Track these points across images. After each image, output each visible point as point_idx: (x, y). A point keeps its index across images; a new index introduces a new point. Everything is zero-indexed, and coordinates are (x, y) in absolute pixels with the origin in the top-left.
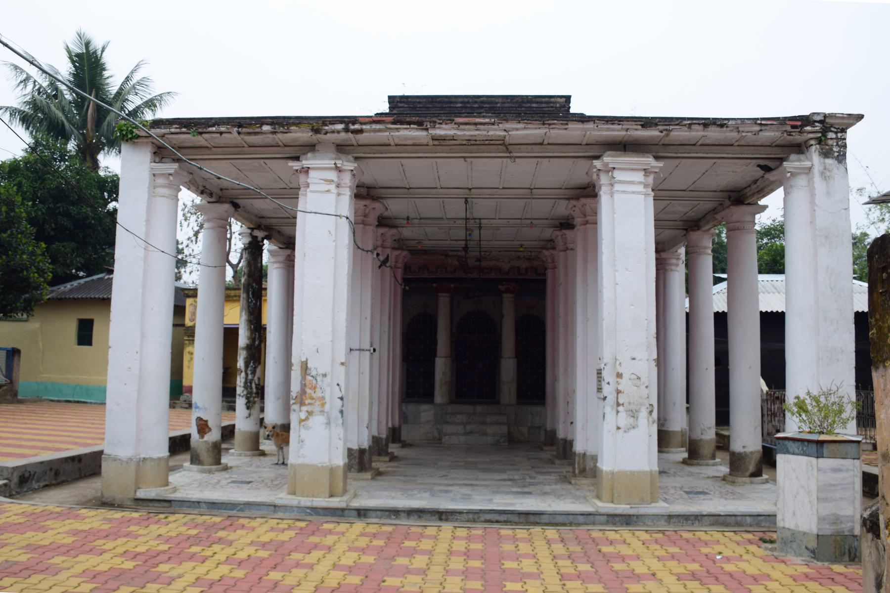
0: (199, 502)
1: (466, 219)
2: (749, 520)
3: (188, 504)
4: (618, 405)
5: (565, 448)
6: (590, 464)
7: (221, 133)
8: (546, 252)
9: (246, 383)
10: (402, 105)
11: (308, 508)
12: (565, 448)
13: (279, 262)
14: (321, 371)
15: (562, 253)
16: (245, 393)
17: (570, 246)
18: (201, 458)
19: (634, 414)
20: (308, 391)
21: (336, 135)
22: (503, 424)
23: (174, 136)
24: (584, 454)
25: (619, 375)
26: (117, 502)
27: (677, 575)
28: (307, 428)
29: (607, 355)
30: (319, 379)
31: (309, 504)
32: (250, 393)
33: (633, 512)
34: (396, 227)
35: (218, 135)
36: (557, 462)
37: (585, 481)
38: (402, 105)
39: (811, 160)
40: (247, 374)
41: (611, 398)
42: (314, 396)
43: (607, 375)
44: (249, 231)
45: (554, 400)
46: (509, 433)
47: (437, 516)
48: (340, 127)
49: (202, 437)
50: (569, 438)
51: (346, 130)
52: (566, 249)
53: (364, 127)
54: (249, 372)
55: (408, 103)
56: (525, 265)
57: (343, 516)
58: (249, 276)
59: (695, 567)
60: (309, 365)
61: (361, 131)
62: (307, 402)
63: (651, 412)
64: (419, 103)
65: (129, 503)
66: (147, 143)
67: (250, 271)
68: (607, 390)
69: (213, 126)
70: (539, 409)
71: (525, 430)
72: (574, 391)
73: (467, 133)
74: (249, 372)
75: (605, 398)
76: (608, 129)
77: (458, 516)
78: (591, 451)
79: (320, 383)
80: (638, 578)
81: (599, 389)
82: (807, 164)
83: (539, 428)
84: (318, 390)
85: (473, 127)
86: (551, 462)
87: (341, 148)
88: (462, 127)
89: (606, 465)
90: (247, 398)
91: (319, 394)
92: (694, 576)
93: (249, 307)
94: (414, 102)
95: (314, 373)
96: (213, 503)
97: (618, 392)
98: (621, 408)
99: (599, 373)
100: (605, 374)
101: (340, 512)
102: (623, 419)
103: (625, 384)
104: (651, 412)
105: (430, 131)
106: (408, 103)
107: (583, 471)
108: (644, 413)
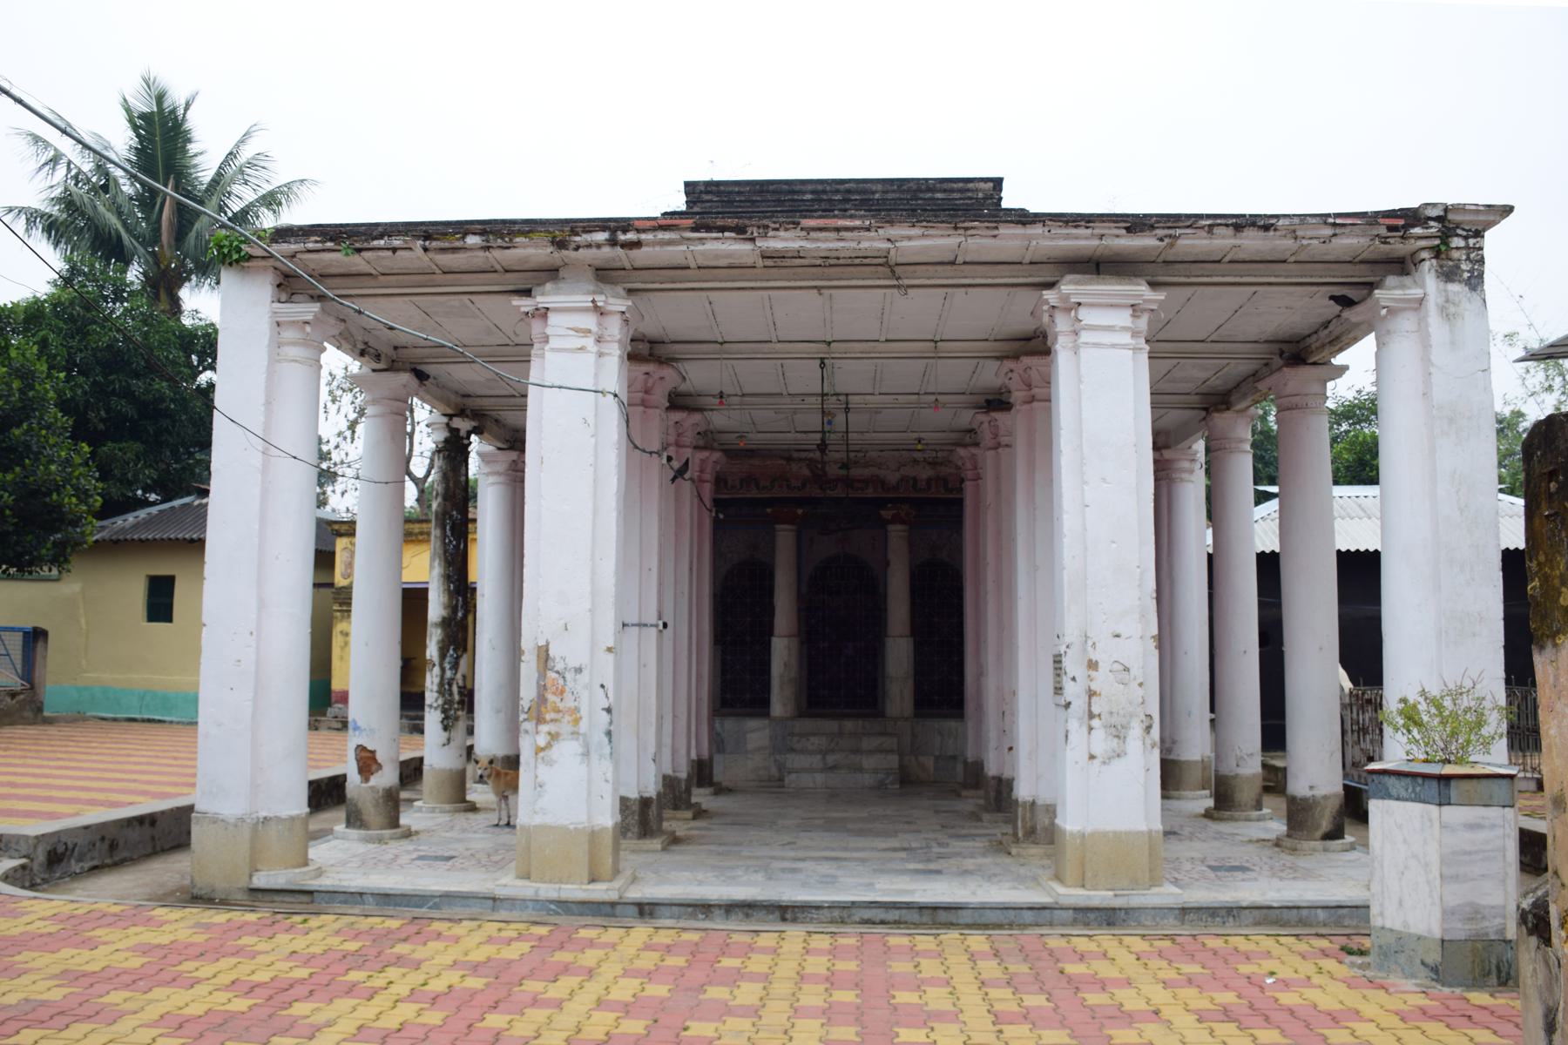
0: (361, 894)
2: (1321, 914)
3: (342, 897)
4: (1091, 716)
5: (999, 792)
6: (1042, 820)
7: (394, 250)
8: (962, 452)
9: (441, 684)
11: (552, 902)
12: (999, 792)
13: (498, 473)
14: (573, 663)
16: (440, 702)
17: (1004, 440)
18: (365, 817)
19: (1118, 733)
20: (551, 697)
21: (594, 250)
25: (1093, 665)
26: (218, 896)
29: (1071, 633)
30: (568, 676)
31: (553, 895)
32: (449, 702)
33: (1118, 903)
34: (701, 410)
35: (390, 253)
37: (1034, 850)
39: (1423, 286)
40: (443, 670)
41: (1079, 704)
42: (561, 706)
43: (1072, 665)
44: (445, 420)
45: (980, 707)
46: (902, 767)
48: (601, 236)
49: (367, 780)
50: (1006, 775)
51: (613, 242)
52: (998, 446)
53: (643, 236)
54: (447, 666)
55: (719, 193)
56: (925, 473)
60: (551, 653)
62: (548, 717)
63: (1148, 728)
64: (739, 193)
65: (239, 896)
66: (265, 268)
67: (447, 489)
68: (1072, 691)
69: (381, 237)
70: (953, 724)
71: (929, 762)
74: (447, 666)
75: (1068, 705)
76: (1067, 237)
78: (1044, 797)
79: (570, 684)
81: (1058, 690)
82: (1416, 292)
83: (954, 758)
84: (567, 695)
85: (833, 235)
86: (975, 817)
87: (604, 274)
88: (813, 235)
89: (1071, 821)
90: (444, 711)
91: (569, 702)
93: (445, 551)
94: (730, 193)
95: (559, 666)
97: (1091, 694)
98: (1095, 723)
99: (1058, 660)
100: (1067, 663)
101: (608, 909)
102: (1101, 741)
103: (1101, 680)
104: (1148, 728)
105: (759, 243)
106: (719, 193)
107: (1031, 832)
108: (1136, 730)
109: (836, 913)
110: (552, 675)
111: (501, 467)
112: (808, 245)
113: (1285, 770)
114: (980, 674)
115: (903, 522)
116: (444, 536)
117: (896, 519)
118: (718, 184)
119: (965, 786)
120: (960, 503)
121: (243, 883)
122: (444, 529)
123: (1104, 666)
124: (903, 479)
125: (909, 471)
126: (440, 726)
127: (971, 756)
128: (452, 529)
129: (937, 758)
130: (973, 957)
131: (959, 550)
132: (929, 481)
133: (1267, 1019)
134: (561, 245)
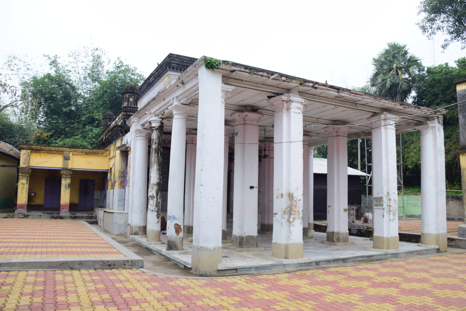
0: (251, 268)
1: (245, 124)
2: (425, 252)
3: (245, 269)
7: (262, 76)
9: (157, 204)
10: (177, 59)
11: (298, 264)
13: (143, 136)
14: (298, 199)
16: (156, 209)
20: (293, 208)
23: (240, 72)
25: (390, 200)
26: (208, 274)
27: (157, 299)
28: (293, 226)
30: (298, 202)
31: (297, 262)
32: (158, 209)
34: (233, 127)
38: (177, 59)
39: (435, 124)
40: (157, 199)
42: (296, 210)
44: (161, 120)
47: (342, 262)
48: (312, 84)
49: (178, 235)
51: (312, 87)
53: (320, 86)
54: (158, 198)
55: (180, 59)
57: (311, 266)
58: (159, 144)
59: (167, 293)
60: (294, 196)
61: (316, 88)
62: (293, 213)
64: (185, 60)
65: (214, 273)
66: (220, 72)
67: (159, 142)
69: (261, 72)
73: (352, 97)
74: (158, 198)
75: (384, 209)
76: (391, 104)
77: (350, 260)
80: (137, 302)
82: (434, 125)
84: (297, 207)
85: (354, 95)
87: (301, 93)
88: (351, 94)
90: (158, 212)
91: (297, 209)
92: (166, 298)
93: (159, 161)
94: (183, 59)
95: (295, 199)
96: (258, 267)
98: (391, 212)
101: (309, 264)
102: (392, 217)
105: (340, 93)
106: (180, 59)
109: (353, 259)
110: (294, 202)
111: (144, 135)
112: (349, 96)
116: (158, 156)
118: (180, 56)
121: (215, 269)
122: (158, 154)
123: (392, 200)
126: (156, 217)
128: (161, 154)
130: (85, 281)
133: (216, 286)
134: (301, 84)
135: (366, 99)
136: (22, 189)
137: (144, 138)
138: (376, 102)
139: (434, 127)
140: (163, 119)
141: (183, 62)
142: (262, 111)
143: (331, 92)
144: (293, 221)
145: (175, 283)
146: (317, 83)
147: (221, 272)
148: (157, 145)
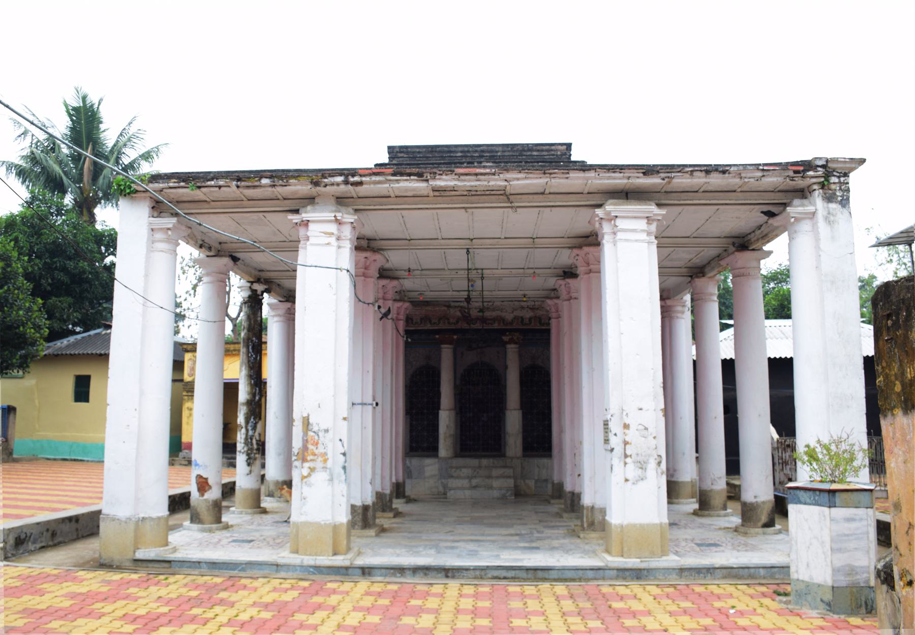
0: (199, 562)
2: (762, 572)
3: (188, 564)
4: (626, 456)
5: (572, 501)
6: (598, 517)
7: (220, 187)
8: (549, 302)
9: (246, 439)
10: (402, 155)
11: (311, 567)
12: (572, 501)
14: (323, 427)
15: (566, 303)
16: (246, 449)
20: (310, 447)
21: (335, 187)
22: (509, 477)
24: (593, 507)
25: (626, 426)
26: (116, 563)
28: (310, 485)
29: (614, 406)
30: (321, 434)
31: (312, 563)
32: (251, 449)
36: (565, 515)
37: (593, 535)
39: (815, 205)
40: (247, 430)
41: (619, 450)
42: (316, 452)
43: (614, 427)
44: (249, 285)
45: (561, 450)
46: (516, 486)
48: (340, 179)
49: (203, 495)
51: (346, 182)
52: (570, 299)
53: (364, 179)
54: (250, 428)
55: (407, 153)
56: (528, 314)
58: (249, 330)
60: (310, 421)
62: (309, 458)
63: (659, 463)
64: (419, 152)
65: (127, 564)
66: (145, 198)
67: (250, 325)
68: (614, 441)
69: (212, 179)
70: (545, 461)
71: (531, 483)
72: (581, 443)
73: (468, 184)
74: (250, 428)
75: (612, 450)
76: (609, 178)
77: (465, 573)
78: (599, 504)
79: (322, 439)
81: (607, 441)
82: (811, 209)
83: (546, 481)
84: (320, 446)
85: (474, 178)
86: (559, 515)
87: (341, 201)
89: (615, 518)
90: (248, 455)
91: (321, 449)
93: (249, 361)
95: (315, 429)
96: (214, 563)
97: (626, 443)
98: (628, 460)
99: (606, 424)
100: (611, 425)
101: (344, 571)
102: (632, 471)
103: (631, 435)
104: (659, 463)
106: (407, 153)
108: (652, 464)
109: (478, 573)
110: (311, 434)
111: (281, 312)
112: (459, 183)
113: (739, 486)
114: (561, 431)
115: (516, 343)
116: (248, 352)
117: (511, 341)
118: (407, 147)
119: (553, 497)
120: (548, 331)
121: (130, 556)
123: (633, 427)
124: (516, 318)
125: (519, 313)
126: (245, 463)
127: (556, 479)
128: (253, 348)
129: (536, 481)
130: (558, 599)
131: (548, 359)
132: (530, 319)
134: (316, 184)
135: (518, 179)
136: (188, 418)
137: (282, 319)
138: (553, 180)
139: (814, 214)
140: (252, 283)
141: (415, 158)
142: (383, 242)
143: (402, 184)
144: (309, 475)
145: (698, 623)
146: (353, 172)
147: (140, 563)
148: (245, 331)
